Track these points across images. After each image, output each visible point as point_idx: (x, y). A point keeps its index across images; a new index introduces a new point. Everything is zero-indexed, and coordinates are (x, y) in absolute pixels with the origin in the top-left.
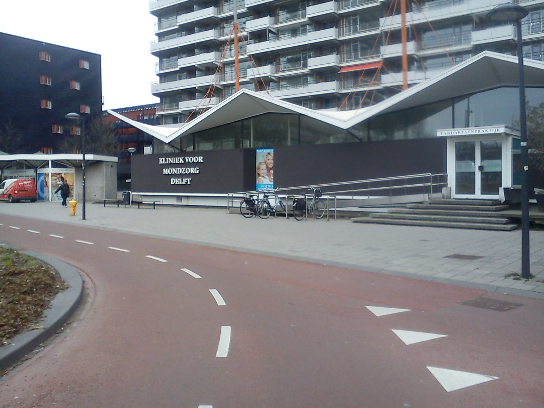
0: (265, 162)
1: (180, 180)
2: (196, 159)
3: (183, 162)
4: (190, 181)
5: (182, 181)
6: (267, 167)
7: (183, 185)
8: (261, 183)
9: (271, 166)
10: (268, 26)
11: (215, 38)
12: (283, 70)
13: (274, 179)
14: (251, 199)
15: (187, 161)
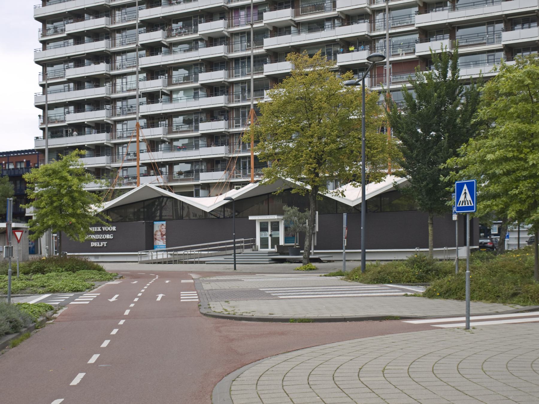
0: (160, 231)
1: (98, 243)
2: (111, 228)
3: (100, 230)
4: (106, 244)
5: (100, 244)
6: (162, 234)
7: (101, 247)
8: (157, 244)
9: (164, 233)
10: (161, 88)
11: (108, 95)
12: (175, 130)
13: (166, 241)
14: (334, 174)
15: (104, 230)
